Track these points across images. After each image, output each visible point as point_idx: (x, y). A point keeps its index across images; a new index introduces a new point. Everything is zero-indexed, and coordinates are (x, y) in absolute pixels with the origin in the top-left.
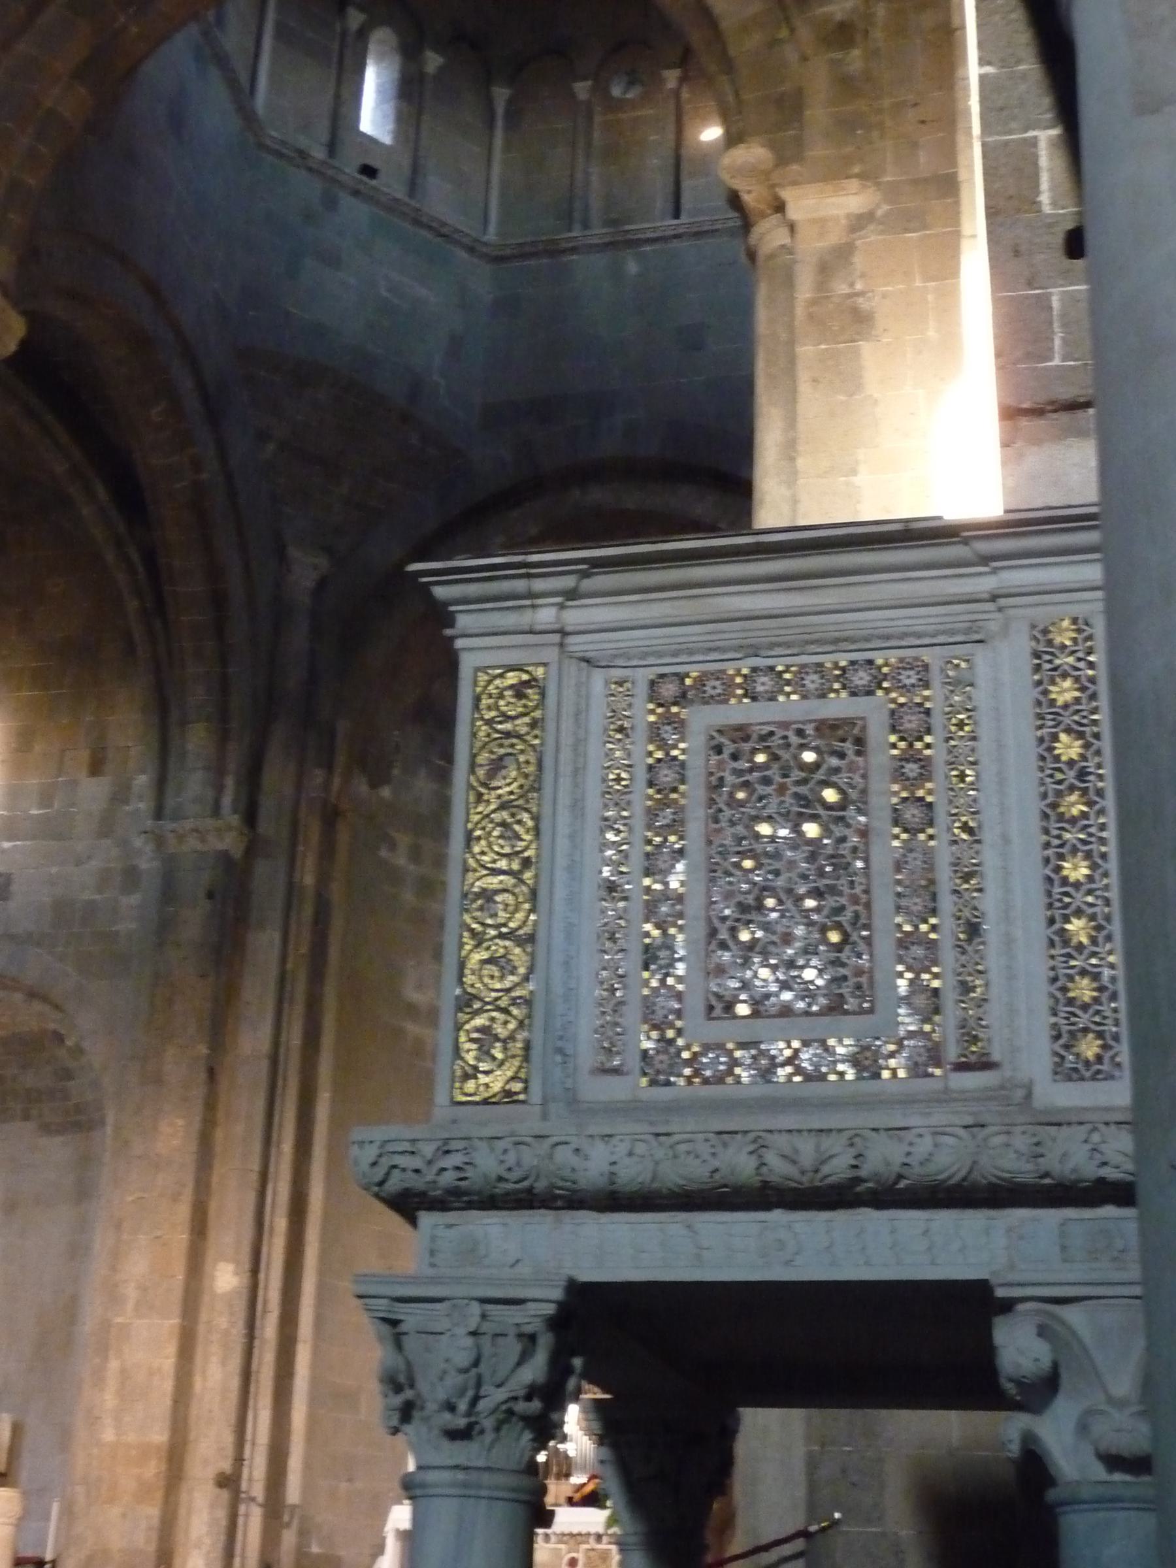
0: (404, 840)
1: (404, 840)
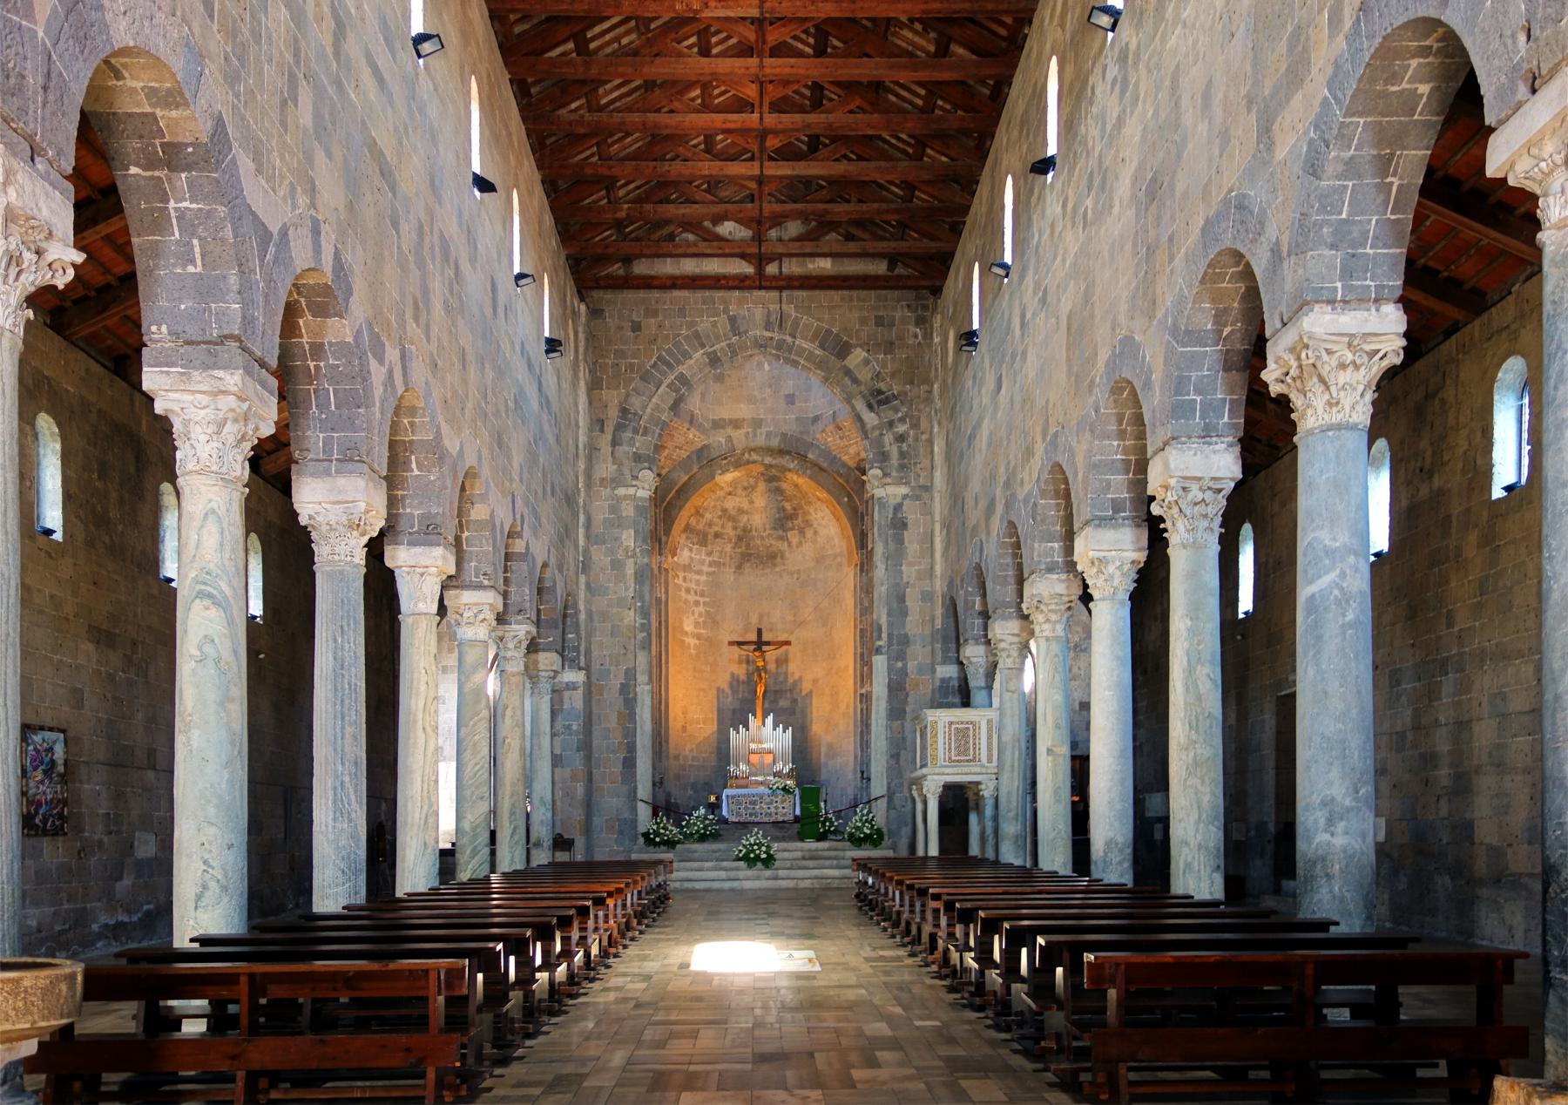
1: (681, 575)
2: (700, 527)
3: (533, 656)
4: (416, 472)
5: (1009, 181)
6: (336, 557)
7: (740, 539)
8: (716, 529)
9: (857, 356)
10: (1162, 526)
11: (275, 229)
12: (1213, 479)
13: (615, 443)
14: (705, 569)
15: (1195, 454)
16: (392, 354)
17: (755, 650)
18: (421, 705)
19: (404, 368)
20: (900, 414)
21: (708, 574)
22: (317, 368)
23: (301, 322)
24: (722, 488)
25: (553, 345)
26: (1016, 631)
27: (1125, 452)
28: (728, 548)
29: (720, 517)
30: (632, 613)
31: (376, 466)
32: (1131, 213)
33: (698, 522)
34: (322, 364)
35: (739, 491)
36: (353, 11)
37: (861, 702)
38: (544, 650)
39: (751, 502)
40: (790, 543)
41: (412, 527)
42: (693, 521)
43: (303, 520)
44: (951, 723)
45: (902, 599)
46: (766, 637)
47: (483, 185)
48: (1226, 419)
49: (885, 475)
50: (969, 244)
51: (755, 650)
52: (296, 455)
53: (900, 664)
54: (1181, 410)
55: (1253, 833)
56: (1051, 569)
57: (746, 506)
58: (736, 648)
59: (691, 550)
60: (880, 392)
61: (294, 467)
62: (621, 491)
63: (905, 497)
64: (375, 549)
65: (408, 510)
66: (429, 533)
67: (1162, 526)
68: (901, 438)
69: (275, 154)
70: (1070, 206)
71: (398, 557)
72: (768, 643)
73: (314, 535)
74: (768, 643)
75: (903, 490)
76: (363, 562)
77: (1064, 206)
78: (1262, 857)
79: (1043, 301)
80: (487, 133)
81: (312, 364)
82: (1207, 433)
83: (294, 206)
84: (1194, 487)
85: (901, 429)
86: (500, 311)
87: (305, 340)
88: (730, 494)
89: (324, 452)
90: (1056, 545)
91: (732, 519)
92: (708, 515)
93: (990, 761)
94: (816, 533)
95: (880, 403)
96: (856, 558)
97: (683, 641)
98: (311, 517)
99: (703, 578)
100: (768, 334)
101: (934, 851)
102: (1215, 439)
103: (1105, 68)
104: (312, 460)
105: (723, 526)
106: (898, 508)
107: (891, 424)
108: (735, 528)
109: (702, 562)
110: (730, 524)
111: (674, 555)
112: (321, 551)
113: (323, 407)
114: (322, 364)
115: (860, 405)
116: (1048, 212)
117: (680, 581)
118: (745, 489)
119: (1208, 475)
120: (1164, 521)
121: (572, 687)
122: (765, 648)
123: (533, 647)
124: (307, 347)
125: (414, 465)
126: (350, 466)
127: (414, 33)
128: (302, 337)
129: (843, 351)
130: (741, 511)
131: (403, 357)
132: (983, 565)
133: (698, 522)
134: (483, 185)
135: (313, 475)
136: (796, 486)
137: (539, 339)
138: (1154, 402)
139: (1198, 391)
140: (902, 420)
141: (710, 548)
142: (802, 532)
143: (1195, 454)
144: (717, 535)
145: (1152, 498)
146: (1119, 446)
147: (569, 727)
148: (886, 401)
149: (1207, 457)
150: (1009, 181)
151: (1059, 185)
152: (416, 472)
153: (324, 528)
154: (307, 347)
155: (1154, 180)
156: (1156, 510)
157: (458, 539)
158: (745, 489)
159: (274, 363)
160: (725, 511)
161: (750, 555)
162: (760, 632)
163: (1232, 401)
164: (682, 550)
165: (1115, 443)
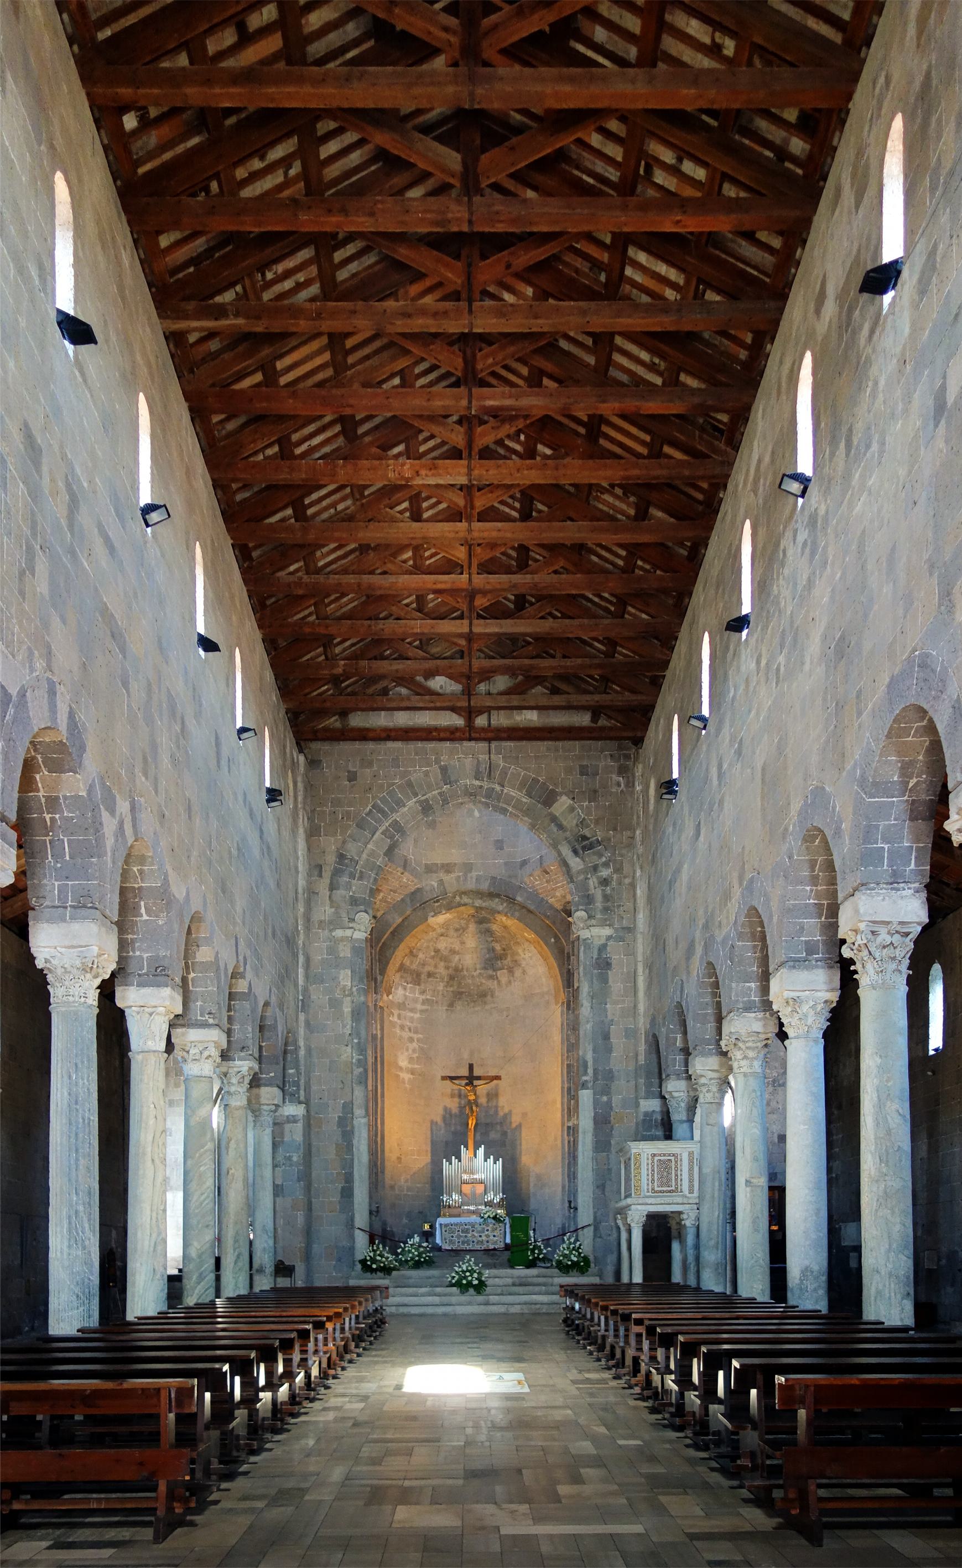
0: (396, 1012)
1: (396, 1012)
2: (414, 967)
3: (255, 1091)
4: (145, 917)
5: (706, 637)
6: (71, 999)
7: (452, 978)
8: (427, 969)
9: (564, 802)
10: (852, 968)
11: (14, 691)
12: (901, 923)
13: (332, 887)
14: (419, 1007)
15: (884, 899)
16: (123, 807)
17: (467, 1084)
18: (150, 1138)
19: (134, 820)
20: (604, 859)
21: (422, 1011)
22: (52, 820)
23: (38, 777)
24: (434, 930)
25: (273, 795)
26: (716, 1068)
27: (818, 896)
28: (441, 987)
29: (433, 957)
30: (349, 1049)
31: (108, 912)
32: (820, 670)
33: (412, 962)
34: (57, 816)
35: (452, 933)
36: (85, 485)
37: (568, 1135)
38: (266, 1085)
39: (463, 943)
40: (499, 982)
41: (141, 969)
42: (407, 962)
43: (40, 964)
44: (655, 1155)
45: (606, 1037)
46: (476, 1073)
47: (208, 645)
48: (913, 866)
49: (590, 917)
50: (668, 698)
51: (467, 1084)
52: (33, 902)
53: (605, 1098)
54: (870, 858)
55: (944, 1262)
56: (748, 1008)
57: (457, 947)
58: (448, 1082)
59: (405, 989)
60: (584, 838)
61: (31, 913)
62: (339, 933)
63: (609, 938)
64: (107, 991)
65: (138, 953)
66: (158, 975)
67: (852, 968)
68: (605, 882)
69: (15, 621)
70: (763, 662)
71: (127, 997)
72: (479, 1078)
73: (50, 978)
74: (479, 1078)
75: (607, 931)
76: (96, 1003)
77: (758, 662)
78: (952, 1285)
79: (739, 753)
80: (211, 595)
81: (48, 817)
82: (895, 880)
83: (32, 670)
84: (883, 931)
85: (605, 873)
86: (224, 762)
87: (41, 794)
88: (442, 935)
89: (59, 899)
90: (753, 985)
91: (445, 959)
92: (421, 956)
93: (691, 1191)
94: (524, 972)
95: (584, 848)
96: (562, 996)
97: (398, 1076)
98: (47, 961)
99: (418, 1015)
100: (477, 783)
101: (638, 1278)
102: (902, 885)
103: (796, 531)
104: (47, 907)
105: (436, 966)
106: (603, 948)
107: (595, 868)
108: (447, 968)
109: (415, 1000)
110: (442, 964)
111: (389, 993)
112: (56, 992)
113: (58, 856)
114: (57, 816)
115: (566, 851)
116: (743, 668)
117: (395, 1019)
118: (457, 930)
119: (895, 920)
120: (854, 963)
121: (292, 1120)
122: (476, 1083)
123: (255, 1082)
124: (43, 800)
125: (143, 910)
126: (84, 912)
127: (142, 504)
128: (38, 791)
129: (549, 799)
130: (453, 952)
131: (133, 809)
132: (684, 1004)
133: (412, 962)
134: (208, 645)
135: (50, 920)
136: (505, 927)
137: (260, 789)
138: (843, 851)
139: (885, 840)
140: (606, 865)
141: (423, 987)
142: (511, 971)
143: (884, 899)
144: (430, 975)
145: (843, 942)
146: (811, 891)
147: (290, 1158)
148: (591, 847)
149: (895, 902)
150: (706, 637)
151: (753, 641)
152: (145, 917)
153: (60, 971)
154: (43, 800)
155: (842, 638)
156: (846, 952)
157: (184, 980)
158: (457, 930)
159: (13, 817)
160: (437, 951)
161: (462, 993)
162: (471, 1067)
163: (918, 849)
164: (397, 989)
165: (808, 888)
